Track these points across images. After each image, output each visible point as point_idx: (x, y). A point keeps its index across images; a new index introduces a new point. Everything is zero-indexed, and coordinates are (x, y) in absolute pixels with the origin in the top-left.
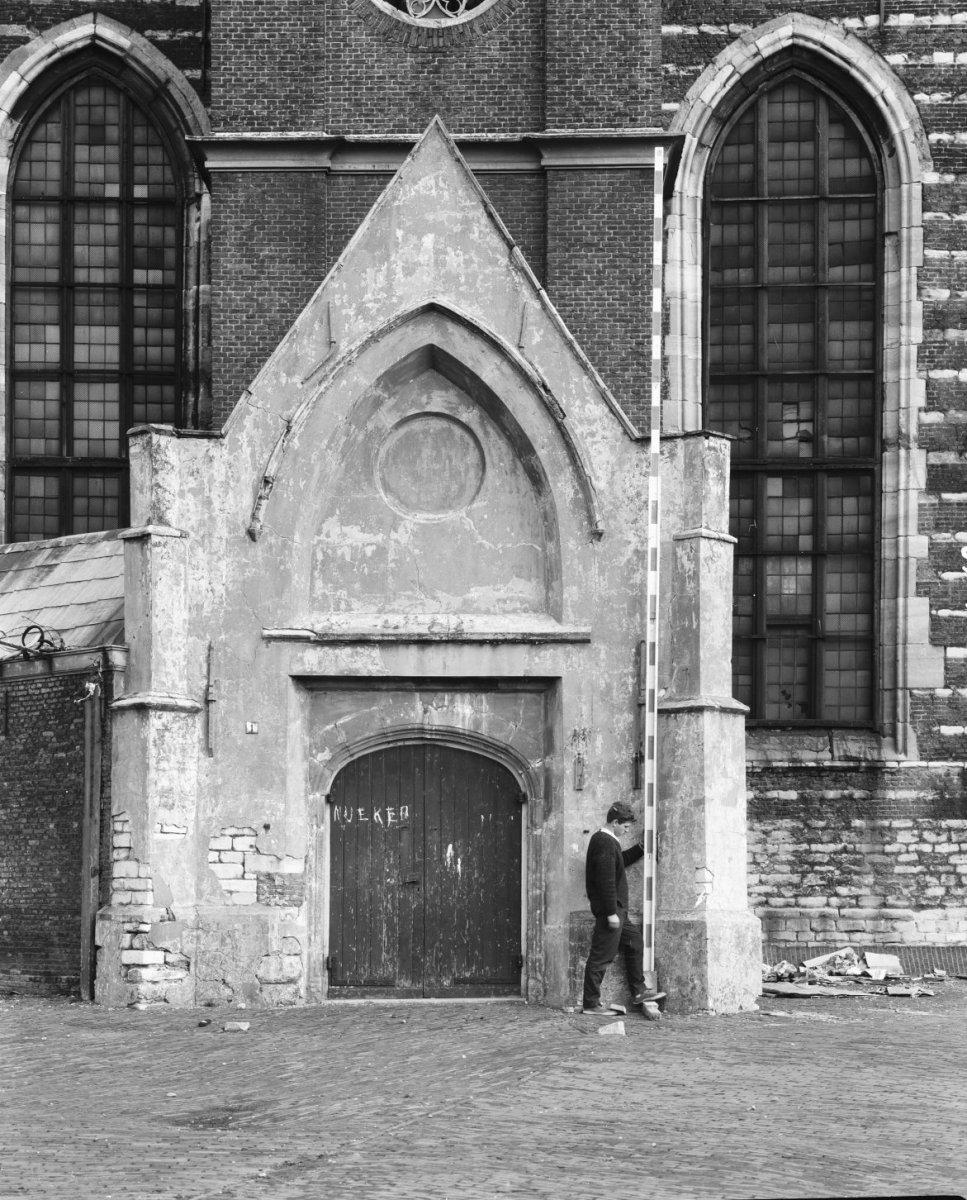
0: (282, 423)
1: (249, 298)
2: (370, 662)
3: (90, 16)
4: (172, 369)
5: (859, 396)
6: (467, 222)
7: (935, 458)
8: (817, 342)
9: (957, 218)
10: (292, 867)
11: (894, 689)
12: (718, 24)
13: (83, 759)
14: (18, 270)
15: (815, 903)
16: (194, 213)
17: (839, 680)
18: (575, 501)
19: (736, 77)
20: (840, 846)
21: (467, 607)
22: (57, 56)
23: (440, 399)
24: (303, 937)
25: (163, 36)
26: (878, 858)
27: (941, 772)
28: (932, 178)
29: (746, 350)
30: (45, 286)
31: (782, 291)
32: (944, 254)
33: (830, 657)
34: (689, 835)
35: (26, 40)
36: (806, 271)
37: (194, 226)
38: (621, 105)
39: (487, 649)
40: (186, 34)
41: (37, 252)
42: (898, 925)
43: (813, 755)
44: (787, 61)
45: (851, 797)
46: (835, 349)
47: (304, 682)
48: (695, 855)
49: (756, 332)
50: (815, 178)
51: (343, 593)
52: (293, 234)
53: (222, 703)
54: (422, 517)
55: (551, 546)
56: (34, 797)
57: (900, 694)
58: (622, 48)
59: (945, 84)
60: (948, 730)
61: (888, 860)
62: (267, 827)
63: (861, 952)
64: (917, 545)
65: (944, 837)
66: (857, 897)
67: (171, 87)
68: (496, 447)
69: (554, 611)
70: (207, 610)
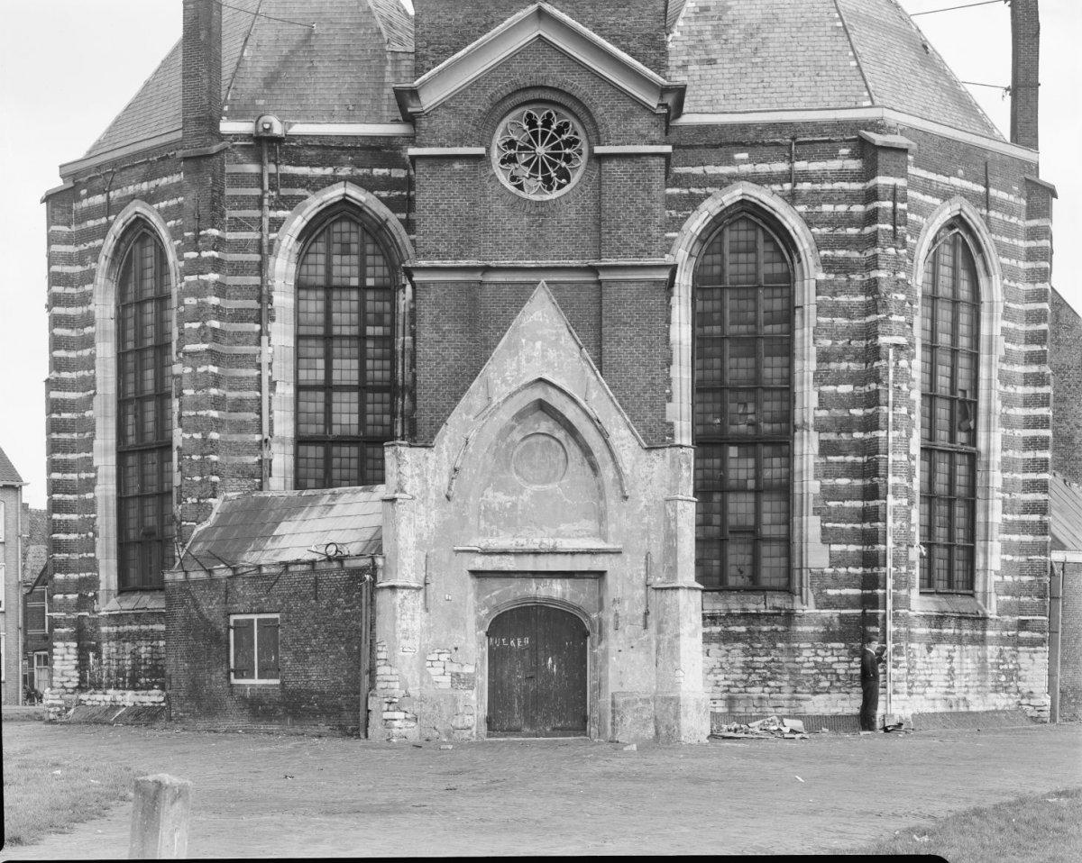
0: (464, 440)
1: (437, 353)
2: (509, 564)
3: (343, 183)
4: (388, 384)
5: (782, 400)
6: (558, 336)
7: (824, 436)
8: (757, 369)
9: (836, 299)
10: (470, 669)
11: (801, 569)
12: (700, 187)
13: (361, 613)
14: (301, 328)
15: (756, 691)
16: (401, 294)
17: (771, 562)
18: (614, 480)
19: (711, 218)
20: (770, 658)
21: (559, 535)
22: (324, 206)
23: (545, 425)
24: (474, 705)
25: (384, 194)
26: (791, 665)
27: (828, 616)
28: (821, 276)
29: (717, 373)
30: (316, 337)
31: (737, 339)
32: (828, 319)
33: (765, 550)
34: (672, 652)
35: (306, 197)
36: (751, 328)
37: (402, 303)
38: (643, 245)
39: (569, 556)
40: (397, 193)
41: (311, 317)
42: (803, 703)
43: (755, 606)
44: (739, 208)
45: (776, 630)
46: (767, 372)
47: (476, 574)
48: (675, 663)
49: (723, 362)
50: (756, 274)
51: (495, 527)
52: (461, 317)
53: (433, 585)
54: (535, 487)
55: (602, 503)
56: (332, 633)
57: (804, 571)
58: (643, 214)
59: (829, 223)
60: (831, 592)
61: (797, 666)
62: (456, 649)
63: (781, 718)
64: (814, 486)
65: (829, 653)
66: (780, 687)
67: (388, 224)
68: (574, 450)
69: (603, 536)
70: (425, 535)
